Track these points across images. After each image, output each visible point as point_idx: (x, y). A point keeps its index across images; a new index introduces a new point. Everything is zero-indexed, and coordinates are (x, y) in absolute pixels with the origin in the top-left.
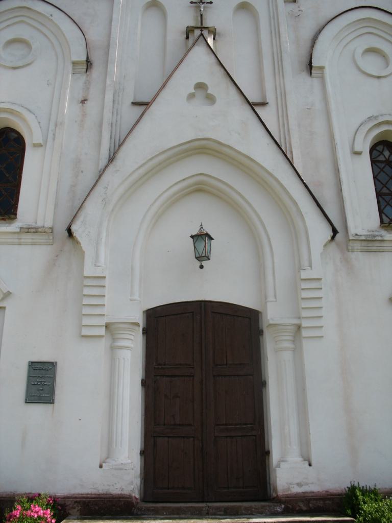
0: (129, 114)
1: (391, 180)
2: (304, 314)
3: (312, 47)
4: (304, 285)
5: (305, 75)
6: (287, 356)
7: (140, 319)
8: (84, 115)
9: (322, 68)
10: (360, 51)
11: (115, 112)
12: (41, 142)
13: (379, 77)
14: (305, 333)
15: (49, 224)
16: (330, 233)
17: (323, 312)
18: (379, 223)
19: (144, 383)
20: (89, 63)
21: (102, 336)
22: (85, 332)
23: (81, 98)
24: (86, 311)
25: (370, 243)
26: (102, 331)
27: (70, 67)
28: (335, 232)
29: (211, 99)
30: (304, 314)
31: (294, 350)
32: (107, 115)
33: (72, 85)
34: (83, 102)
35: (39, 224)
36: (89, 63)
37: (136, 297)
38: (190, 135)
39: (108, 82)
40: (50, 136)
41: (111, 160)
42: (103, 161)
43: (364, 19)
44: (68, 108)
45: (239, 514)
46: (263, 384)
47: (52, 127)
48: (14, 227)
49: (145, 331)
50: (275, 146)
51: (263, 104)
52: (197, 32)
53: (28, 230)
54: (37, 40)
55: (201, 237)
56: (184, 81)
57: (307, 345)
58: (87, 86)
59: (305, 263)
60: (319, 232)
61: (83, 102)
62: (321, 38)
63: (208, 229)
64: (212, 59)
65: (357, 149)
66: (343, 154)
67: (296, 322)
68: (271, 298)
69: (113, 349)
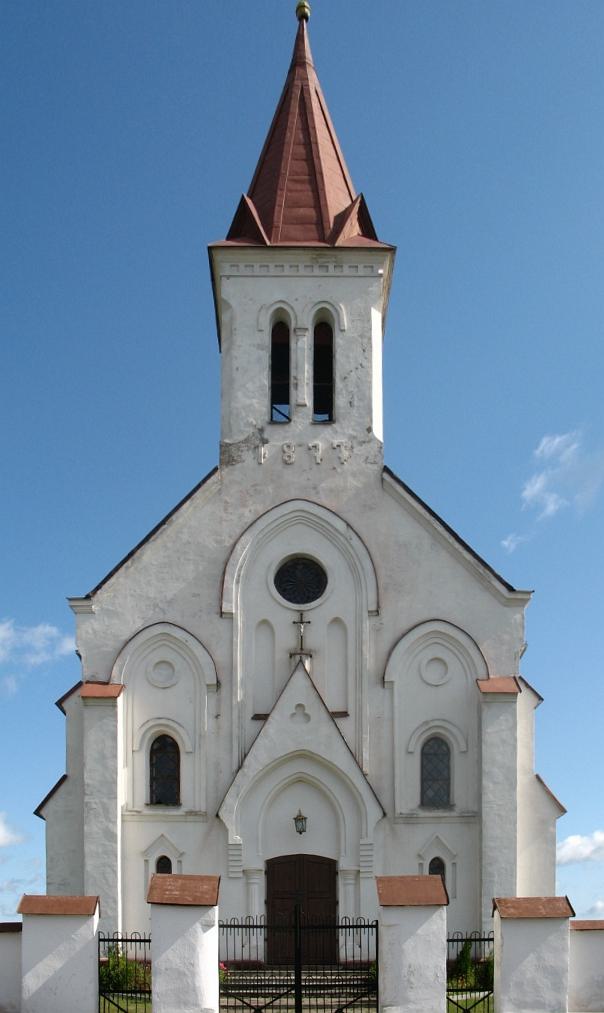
0: (251, 727)
1: (253, 1011)
2: (362, 864)
3: (388, 660)
4: (362, 848)
5: (379, 688)
6: (351, 888)
7: (262, 866)
8: (219, 728)
9: (392, 682)
10: (425, 662)
11: (241, 727)
12: (191, 750)
13: (437, 686)
14: (361, 875)
15: (203, 810)
16: (381, 814)
17: (373, 859)
18: (419, 803)
19: (266, 902)
20: (218, 684)
21: (239, 878)
22: (231, 875)
23: (215, 714)
24: (231, 863)
25: (410, 819)
26: (241, 875)
27: (205, 689)
28: (385, 814)
29: (307, 717)
30: (362, 864)
31: (355, 884)
32: (236, 731)
33: (208, 702)
34: (217, 716)
35: (197, 809)
36: (218, 684)
37: (261, 854)
38: (292, 748)
39: (234, 703)
40: (197, 745)
41: (240, 768)
42: (235, 767)
43: (429, 633)
44: (208, 723)
45: (475, 809)
46: (337, 903)
47: (197, 737)
48: (180, 811)
49: (266, 873)
50: (349, 754)
51: (345, 714)
52: (298, 658)
53: (190, 813)
54: (178, 664)
55: (300, 819)
56: (287, 704)
57: (362, 882)
58: (219, 701)
59: (364, 833)
60: (373, 812)
61: (217, 716)
62: (393, 654)
63: (304, 814)
64: (309, 683)
65: (410, 750)
66: (400, 754)
67: (357, 868)
68: (343, 854)
69: (248, 884)
